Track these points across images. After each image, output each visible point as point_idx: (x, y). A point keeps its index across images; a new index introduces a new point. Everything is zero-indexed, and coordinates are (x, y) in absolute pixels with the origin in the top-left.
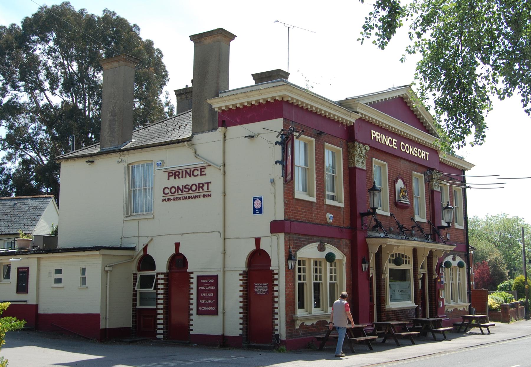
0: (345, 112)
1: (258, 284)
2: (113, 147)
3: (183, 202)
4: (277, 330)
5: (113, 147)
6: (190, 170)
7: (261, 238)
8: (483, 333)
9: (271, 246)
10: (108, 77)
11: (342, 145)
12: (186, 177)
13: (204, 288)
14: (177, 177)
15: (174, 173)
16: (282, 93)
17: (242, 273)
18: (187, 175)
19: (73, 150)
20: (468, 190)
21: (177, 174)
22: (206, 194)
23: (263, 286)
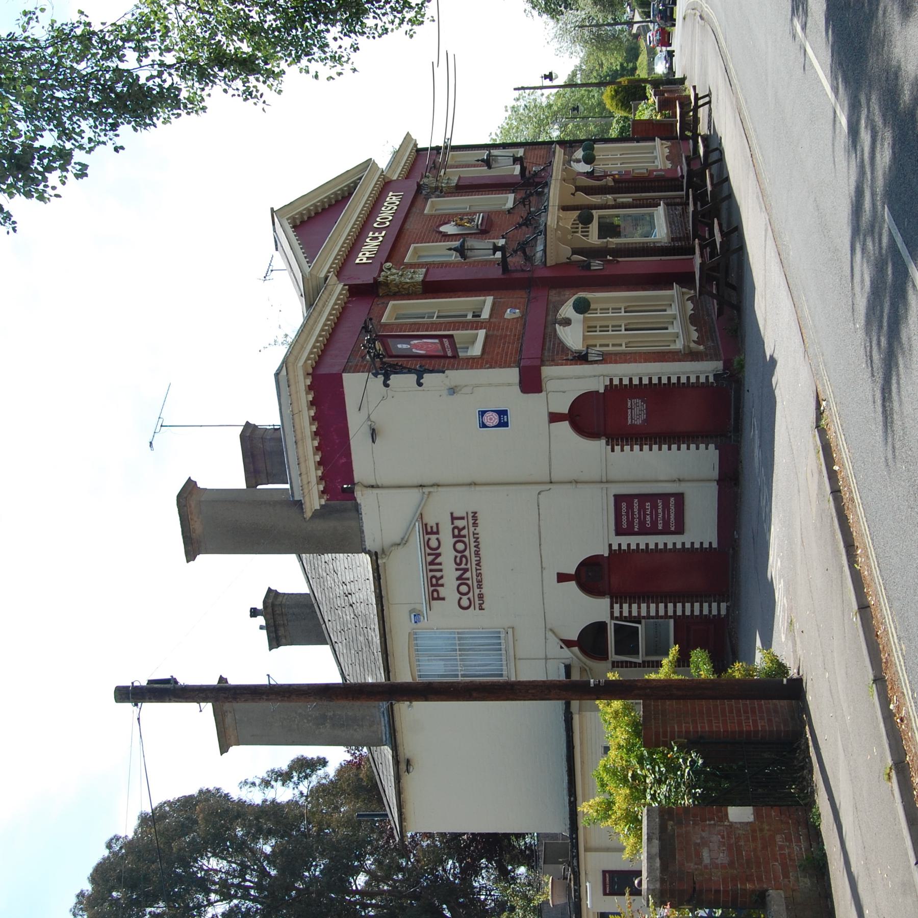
0: (327, 293)
1: (629, 417)
2: (382, 719)
3: (485, 570)
4: (707, 377)
5: (382, 719)
6: (429, 554)
7: (550, 411)
8: (709, 102)
9: (564, 392)
10: (253, 736)
11: (383, 303)
12: (440, 564)
13: (636, 521)
14: (440, 582)
15: (433, 588)
16: (301, 373)
17: (610, 447)
18: (437, 561)
19: (387, 815)
20: (454, 143)
21: (434, 581)
22: (471, 522)
23: (631, 408)
